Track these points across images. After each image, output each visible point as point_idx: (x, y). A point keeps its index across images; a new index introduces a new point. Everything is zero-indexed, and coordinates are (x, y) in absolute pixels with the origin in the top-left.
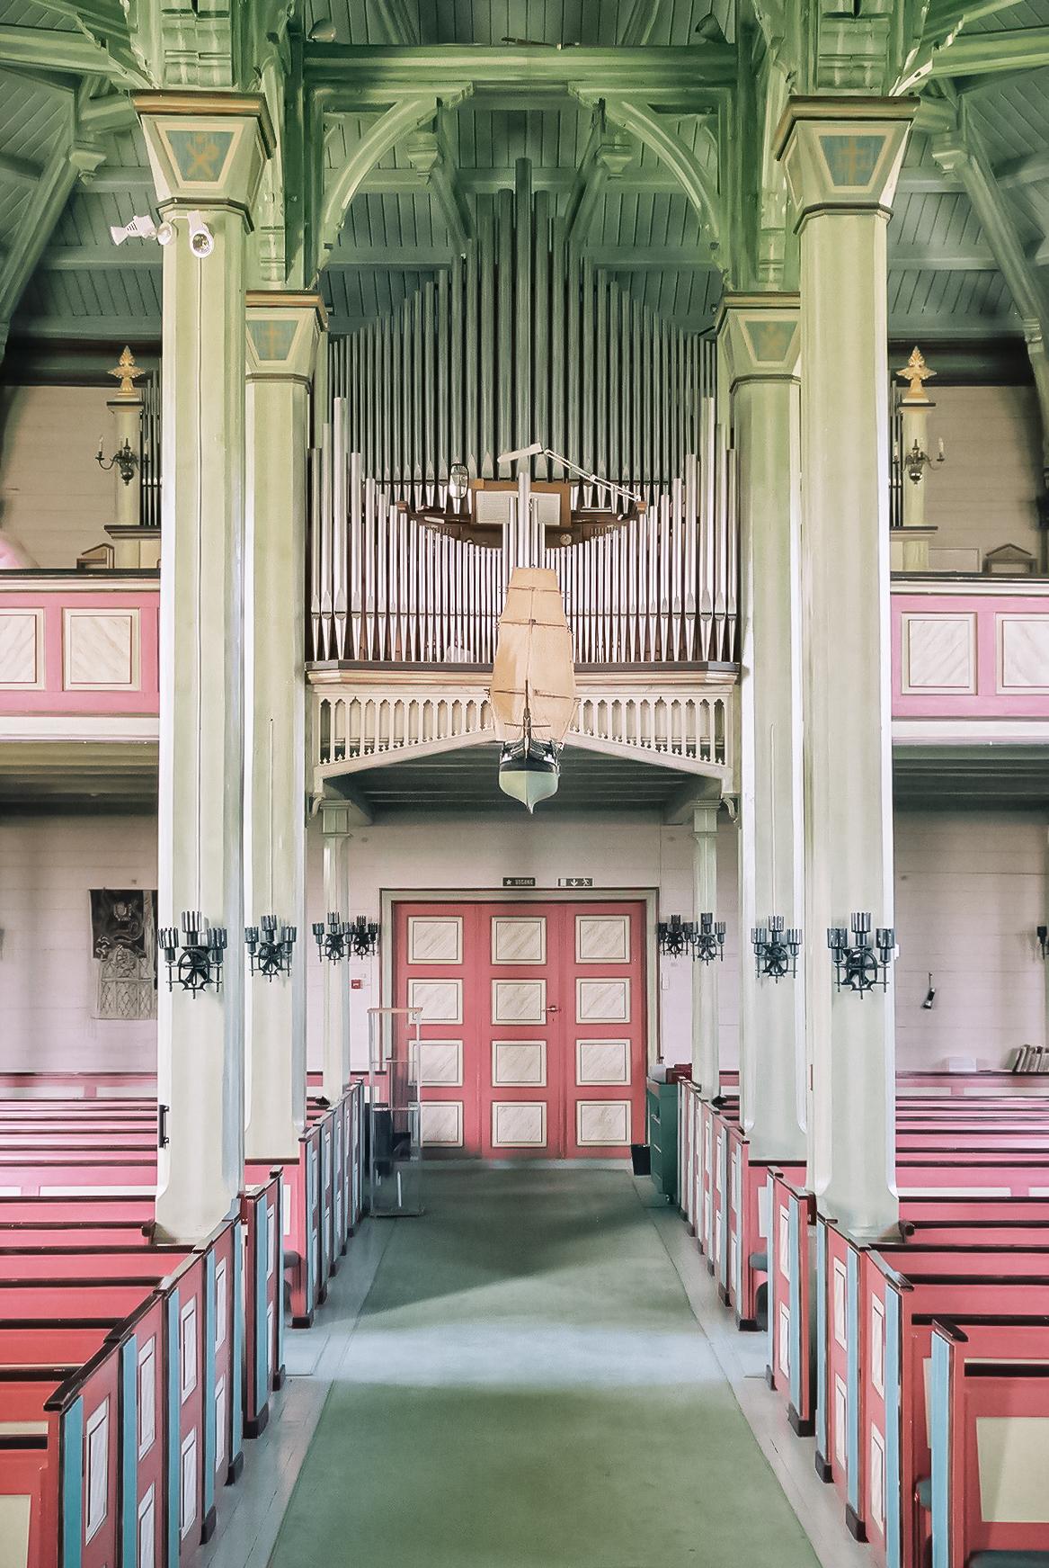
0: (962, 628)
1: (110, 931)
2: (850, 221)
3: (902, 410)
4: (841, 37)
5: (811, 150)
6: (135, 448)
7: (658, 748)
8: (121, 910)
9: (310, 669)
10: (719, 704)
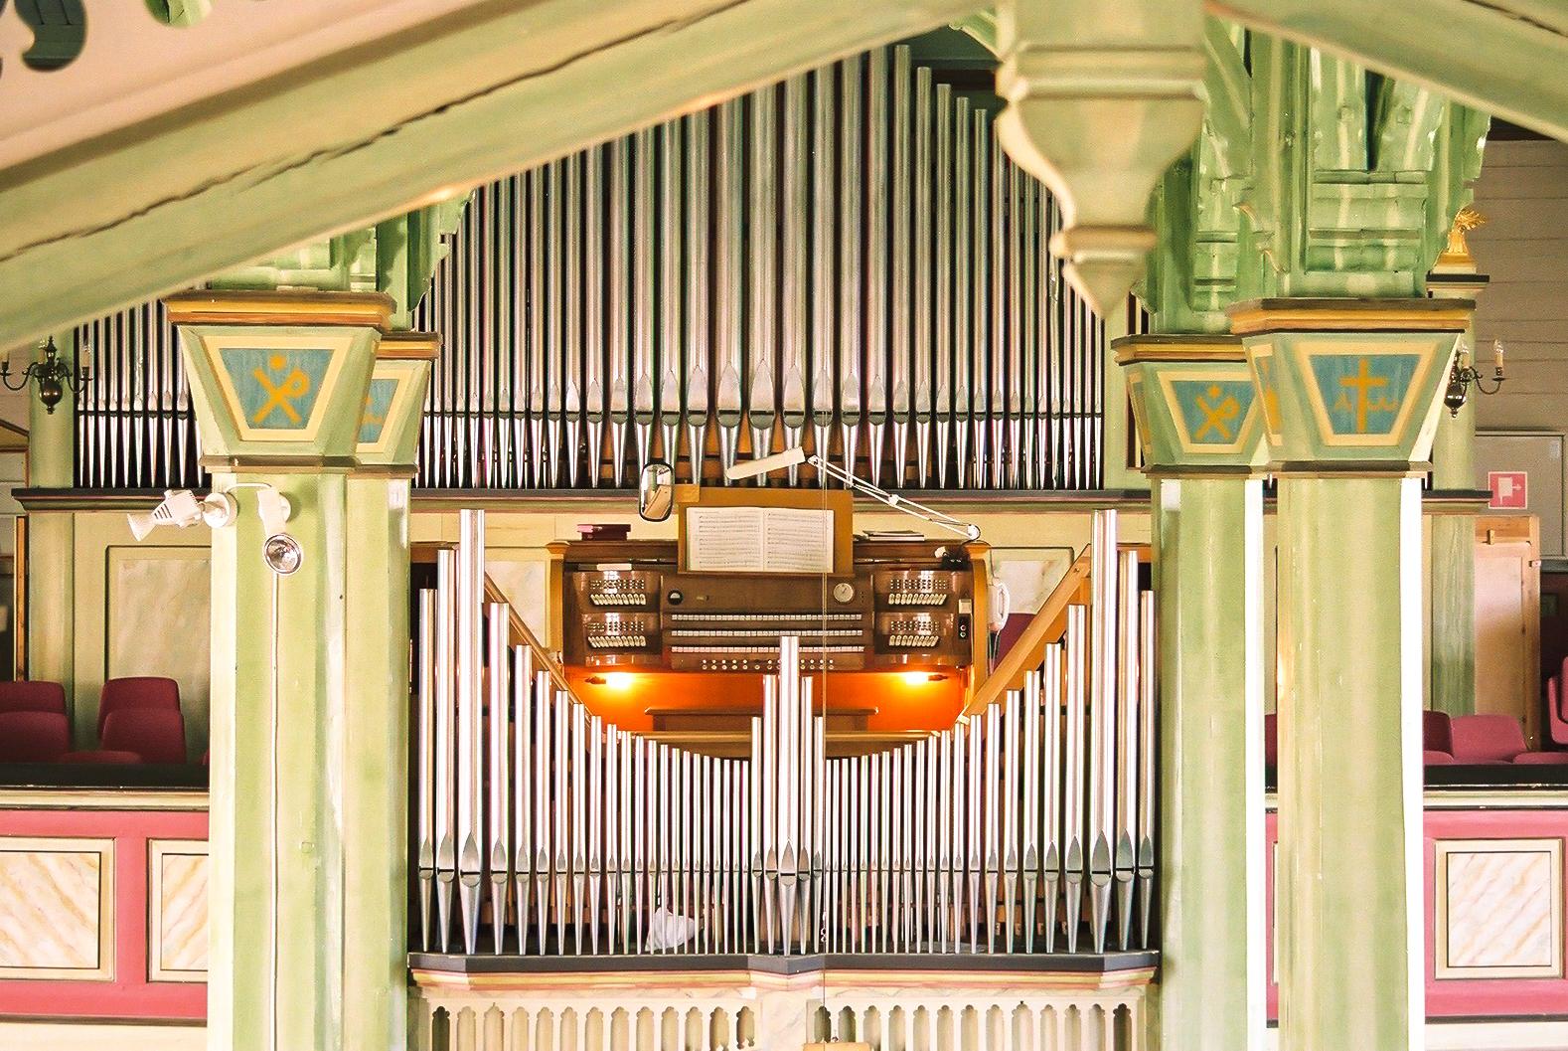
2: (1362, 489)
4: (1345, 207)
5: (1298, 380)
9: (416, 964)
10: (1122, 1012)
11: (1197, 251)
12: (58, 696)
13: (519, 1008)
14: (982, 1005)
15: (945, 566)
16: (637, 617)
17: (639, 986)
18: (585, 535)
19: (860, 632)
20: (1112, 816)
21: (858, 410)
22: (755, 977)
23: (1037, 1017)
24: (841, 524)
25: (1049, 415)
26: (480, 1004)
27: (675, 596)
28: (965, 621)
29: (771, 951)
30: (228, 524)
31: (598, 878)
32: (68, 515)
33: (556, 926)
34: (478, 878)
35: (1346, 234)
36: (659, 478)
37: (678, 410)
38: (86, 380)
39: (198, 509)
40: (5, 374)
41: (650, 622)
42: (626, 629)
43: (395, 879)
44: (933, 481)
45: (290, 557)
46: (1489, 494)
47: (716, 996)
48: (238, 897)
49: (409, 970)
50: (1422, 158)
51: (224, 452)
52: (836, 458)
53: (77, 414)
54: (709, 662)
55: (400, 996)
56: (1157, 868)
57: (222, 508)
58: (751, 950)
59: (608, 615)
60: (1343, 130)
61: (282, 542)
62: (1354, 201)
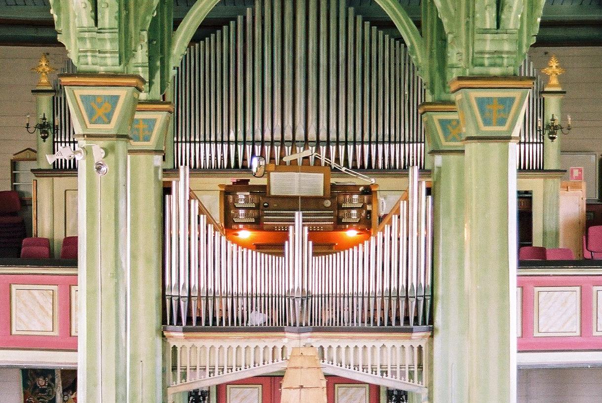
0: (571, 297)
1: (34, 393)
2: (495, 146)
3: (544, 96)
4: (488, 43)
5: (470, 107)
6: (49, 119)
7: (382, 372)
8: (41, 382)
9: (165, 329)
10: (420, 348)
11: (448, 70)
12: (47, 243)
13: (203, 346)
14: (369, 345)
15: (363, 193)
16: (251, 211)
17: (245, 338)
18: (234, 183)
19: (332, 217)
20: (417, 278)
21: (336, 140)
22: (287, 334)
23: (389, 349)
24: (326, 179)
25: (404, 142)
26: (188, 344)
27: (266, 204)
28: (369, 212)
29: (292, 325)
30: (83, 159)
31: (231, 299)
32: (51, 178)
33: (216, 317)
34: (187, 298)
35: (489, 53)
36: (261, 162)
37: (270, 140)
38: (57, 130)
39: (73, 153)
40: (27, 128)
41: (256, 213)
42: (247, 215)
43: (157, 298)
44: (362, 166)
45: (104, 169)
46: (565, 171)
47: (273, 342)
48: (88, 293)
49: (162, 332)
50: (515, 24)
51: (82, 133)
52: (328, 155)
53: (54, 142)
54: (278, 228)
55: (159, 340)
56: (432, 296)
57: (81, 153)
58: (286, 325)
59: (240, 210)
60: (487, 14)
61: (100, 164)
62: (492, 40)
